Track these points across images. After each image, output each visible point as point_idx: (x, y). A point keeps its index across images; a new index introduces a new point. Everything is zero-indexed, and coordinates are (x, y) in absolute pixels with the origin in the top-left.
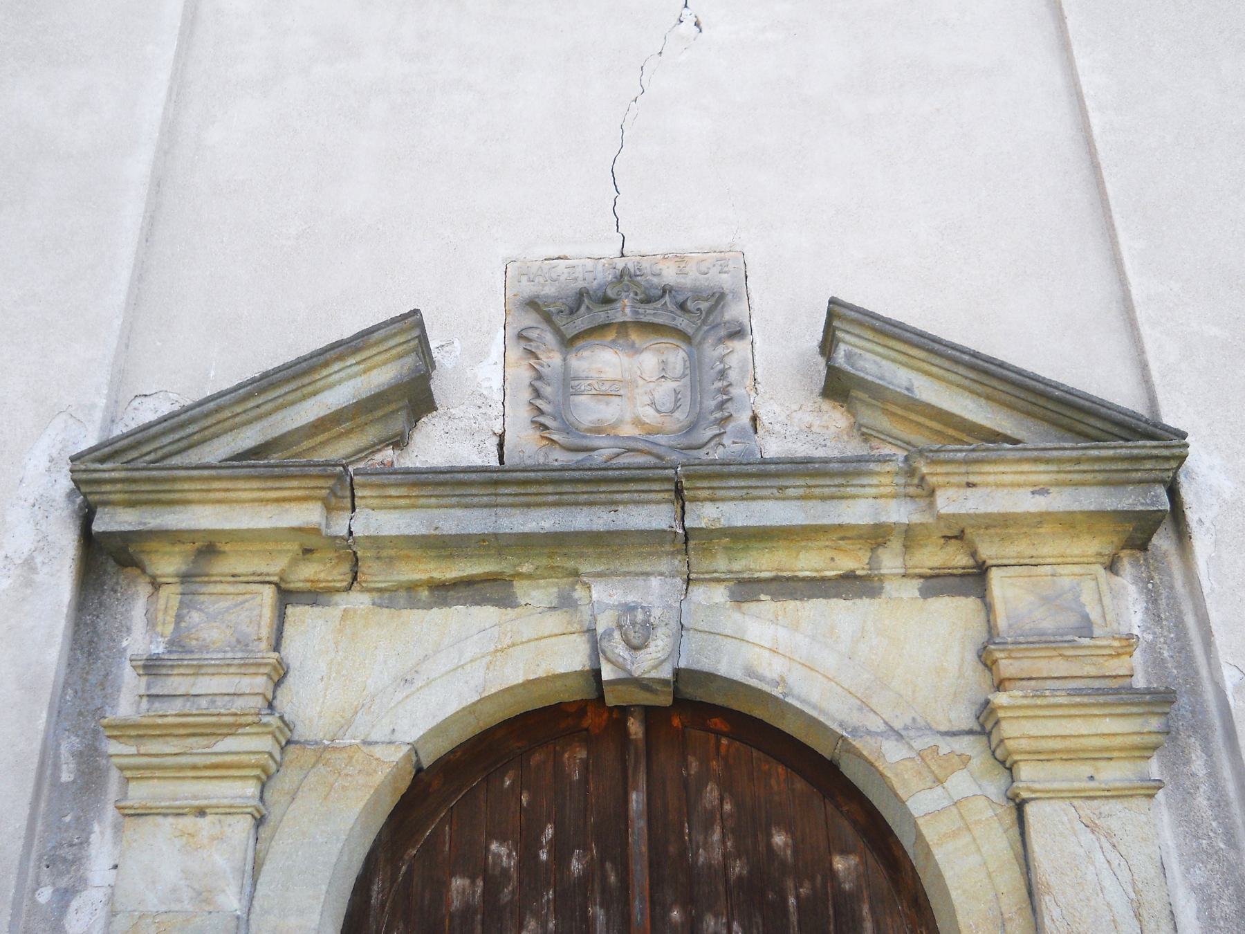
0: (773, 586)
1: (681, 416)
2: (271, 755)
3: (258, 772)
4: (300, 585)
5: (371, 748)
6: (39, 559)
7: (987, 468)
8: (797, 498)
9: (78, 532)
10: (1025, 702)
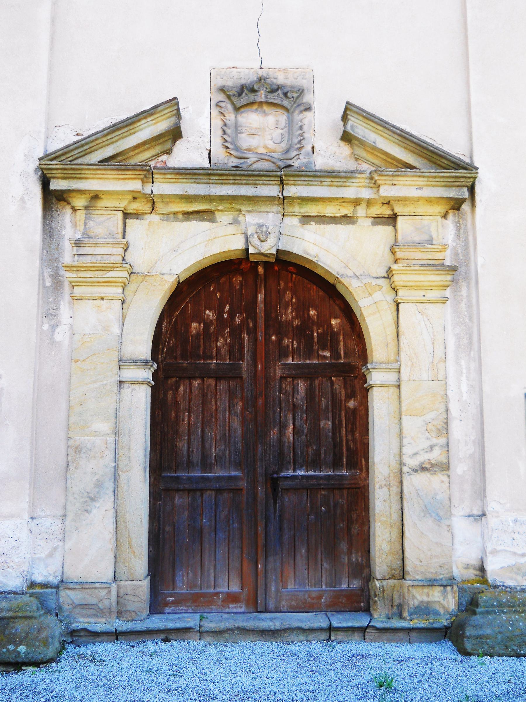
0: (316, 219)
1: (284, 145)
2: (127, 278)
3: (122, 284)
4: (131, 211)
5: (163, 276)
6: (26, 198)
7: (400, 178)
8: (327, 186)
9: (41, 187)
10: (403, 268)
